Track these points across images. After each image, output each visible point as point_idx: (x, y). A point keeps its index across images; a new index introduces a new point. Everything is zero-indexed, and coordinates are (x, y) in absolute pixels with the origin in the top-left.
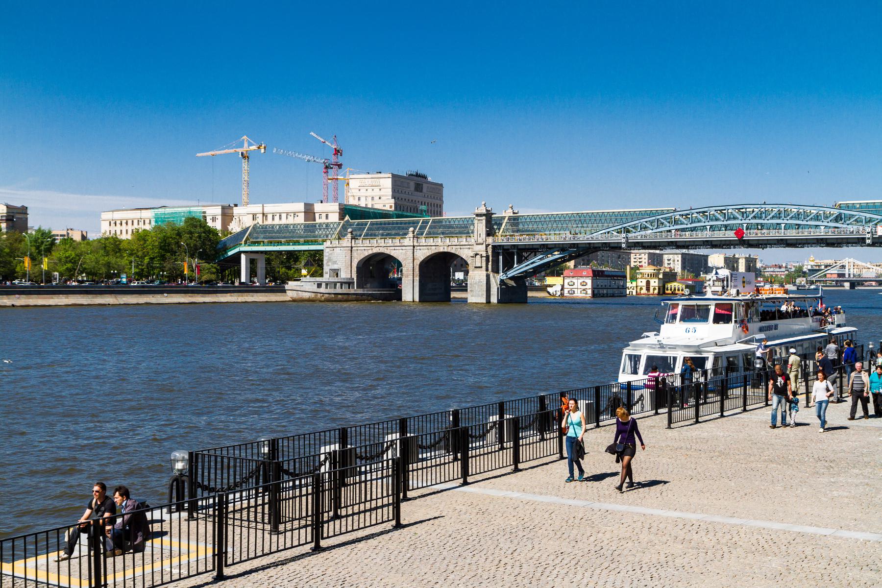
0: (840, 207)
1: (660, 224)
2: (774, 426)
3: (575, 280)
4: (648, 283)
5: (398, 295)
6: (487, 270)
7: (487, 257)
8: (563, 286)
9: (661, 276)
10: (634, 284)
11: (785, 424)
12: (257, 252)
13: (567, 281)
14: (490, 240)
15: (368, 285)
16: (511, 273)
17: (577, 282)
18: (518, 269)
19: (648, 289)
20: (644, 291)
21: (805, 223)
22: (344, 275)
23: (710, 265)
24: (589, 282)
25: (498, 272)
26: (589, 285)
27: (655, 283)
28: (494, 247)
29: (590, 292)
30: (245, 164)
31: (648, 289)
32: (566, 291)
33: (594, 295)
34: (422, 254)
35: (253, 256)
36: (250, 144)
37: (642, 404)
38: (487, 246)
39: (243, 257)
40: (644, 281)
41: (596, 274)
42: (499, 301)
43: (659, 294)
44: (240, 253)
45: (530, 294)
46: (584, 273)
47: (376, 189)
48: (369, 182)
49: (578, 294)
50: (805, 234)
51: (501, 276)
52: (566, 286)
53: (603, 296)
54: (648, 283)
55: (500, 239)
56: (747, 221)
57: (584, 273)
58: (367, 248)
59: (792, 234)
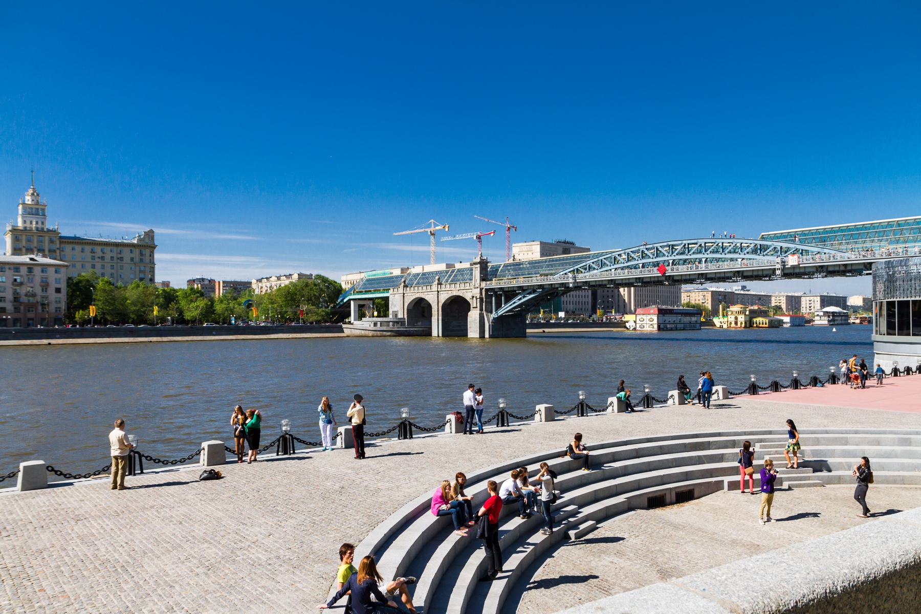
0: (763, 238)
1: (603, 265)
2: (115, 487)
3: (644, 317)
4: (736, 318)
5: (429, 334)
6: (481, 310)
7: (481, 299)
8: (635, 322)
9: (747, 313)
10: (726, 319)
11: (123, 487)
12: (365, 299)
13: (639, 317)
14: (484, 284)
15: (419, 323)
16: (500, 312)
17: (647, 318)
18: (505, 309)
19: (736, 323)
20: (733, 325)
21: (723, 256)
22: (400, 316)
23: (848, 304)
24: (655, 318)
25: (491, 312)
26: (655, 321)
27: (741, 318)
28: (487, 290)
29: (656, 326)
30: (432, 237)
31: (736, 323)
32: (638, 326)
33: (659, 328)
34: (444, 297)
35: (362, 303)
36: (436, 225)
37: (297, 439)
38: (481, 290)
39: (352, 302)
40: (733, 317)
41: (661, 312)
42: (491, 337)
43: (745, 327)
44: (350, 300)
45: (528, 331)
46: (652, 311)
47: (530, 253)
48: (525, 248)
49: (647, 329)
50: (726, 267)
51: (494, 315)
52: (638, 321)
53: (667, 330)
54: (736, 318)
55: (494, 284)
56: (673, 258)
57: (652, 311)
58: (412, 295)
59: (712, 268)
